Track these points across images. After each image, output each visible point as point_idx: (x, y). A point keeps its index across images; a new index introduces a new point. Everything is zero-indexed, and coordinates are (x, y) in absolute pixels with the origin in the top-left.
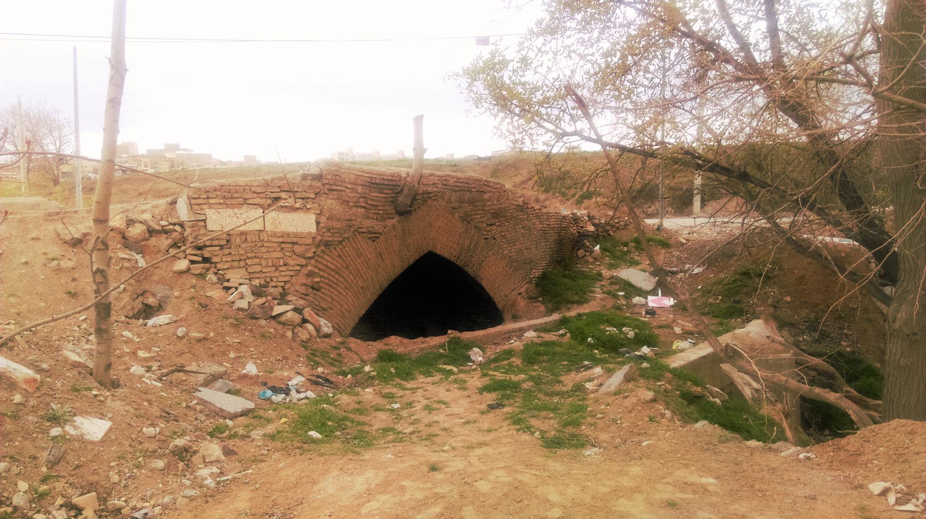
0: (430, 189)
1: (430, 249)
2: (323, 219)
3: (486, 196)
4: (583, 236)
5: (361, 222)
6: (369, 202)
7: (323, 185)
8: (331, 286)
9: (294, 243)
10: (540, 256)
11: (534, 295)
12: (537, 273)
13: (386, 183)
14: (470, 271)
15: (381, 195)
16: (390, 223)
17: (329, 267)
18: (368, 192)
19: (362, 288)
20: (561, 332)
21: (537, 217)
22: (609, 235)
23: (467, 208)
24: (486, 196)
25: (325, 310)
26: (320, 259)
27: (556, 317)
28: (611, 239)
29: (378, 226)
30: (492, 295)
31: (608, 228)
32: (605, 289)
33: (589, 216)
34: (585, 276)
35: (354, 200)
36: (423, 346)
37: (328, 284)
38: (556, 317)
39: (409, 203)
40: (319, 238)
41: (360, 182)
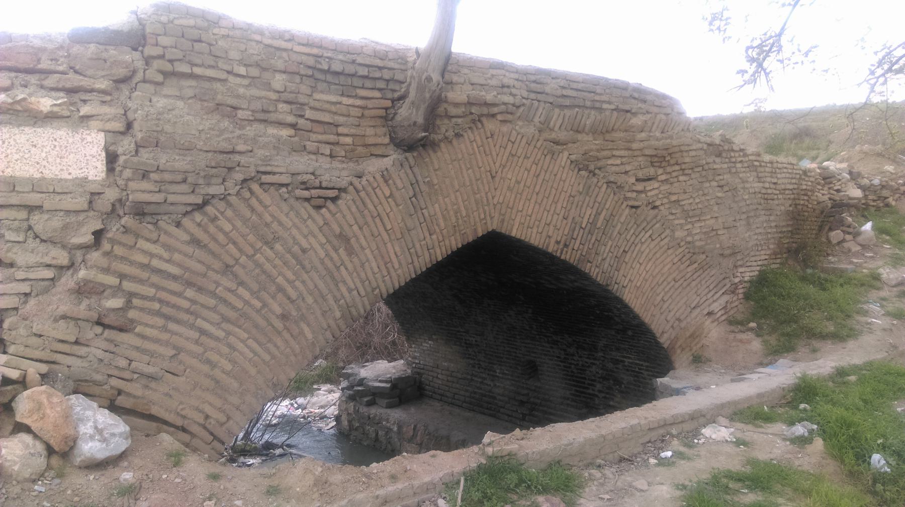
0: (489, 97)
1: (493, 225)
2: (125, 146)
3: (637, 121)
4: (840, 206)
5: (266, 160)
6: (309, 113)
7: (148, 61)
8: (168, 318)
9: (31, 209)
10: (755, 244)
11: (739, 317)
12: (748, 273)
13: (363, 71)
14: (593, 271)
15: (346, 101)
16: (373, 166)
17: (158, 271)
18: (304, 89)
19: (284, 317)
20: (800, 430)
21: (752, 167)
22: (887, 205)
23: (589, 143)
24: (637, 121)
25: (151, 377)
26: (119, 251)
27: (781, 375)
28: (892, 213)
29: (334, 173)
30: (646, 318)
31: (885, 193)
32: (890, 308)
33: (850, 173)
34: (845, 279)
35: (257, 105)
36: (391, 489)
37: (158, 313)
38: (781, 375)
39: (420, 120)
40: (112, 194)
41: (280, 65)
